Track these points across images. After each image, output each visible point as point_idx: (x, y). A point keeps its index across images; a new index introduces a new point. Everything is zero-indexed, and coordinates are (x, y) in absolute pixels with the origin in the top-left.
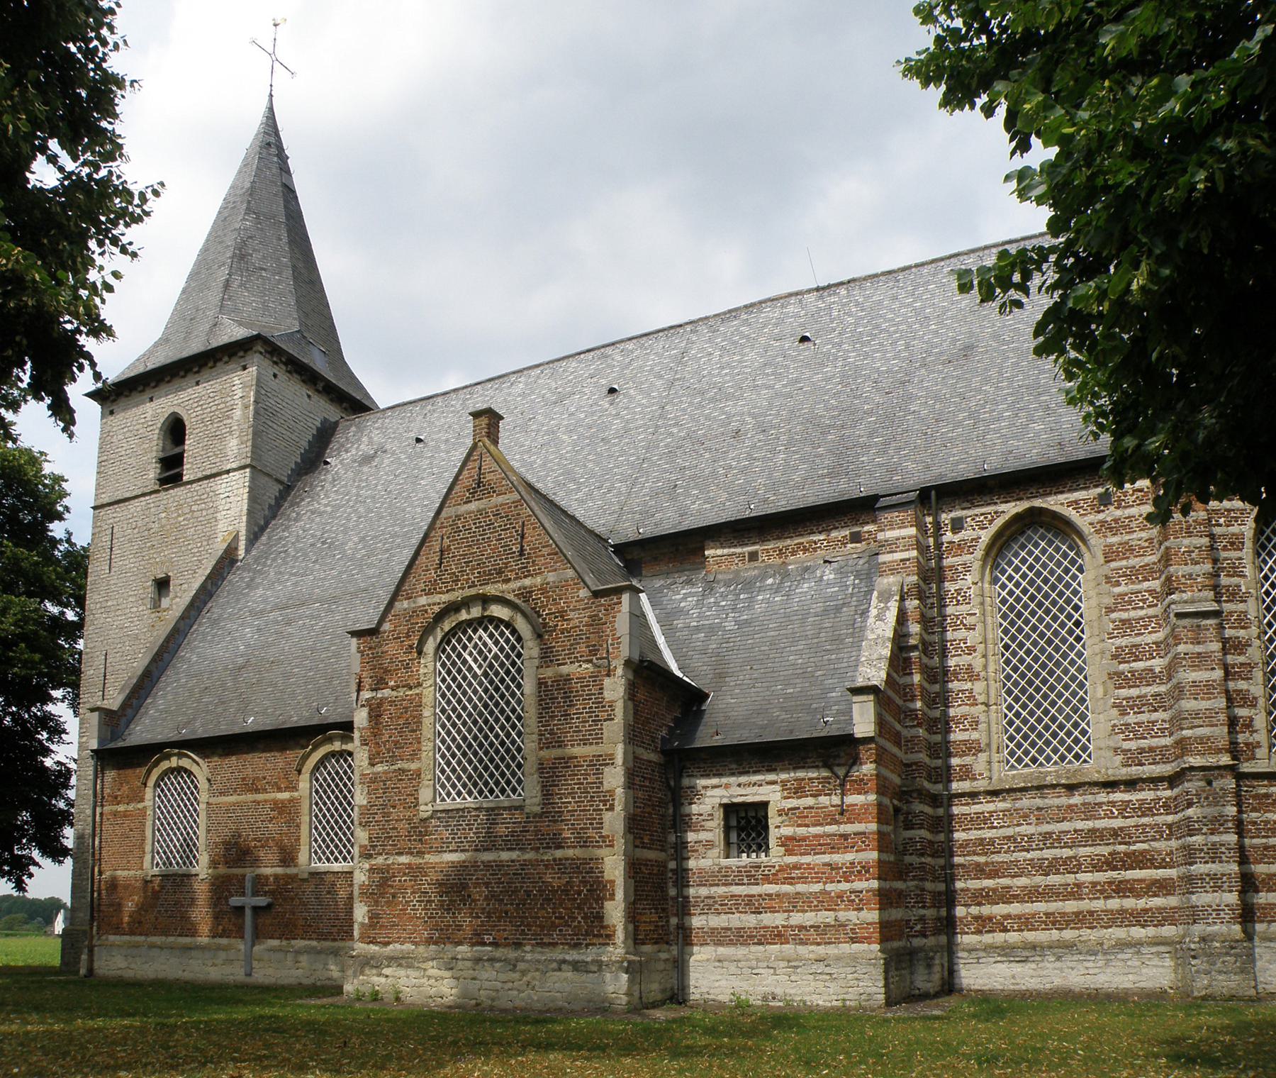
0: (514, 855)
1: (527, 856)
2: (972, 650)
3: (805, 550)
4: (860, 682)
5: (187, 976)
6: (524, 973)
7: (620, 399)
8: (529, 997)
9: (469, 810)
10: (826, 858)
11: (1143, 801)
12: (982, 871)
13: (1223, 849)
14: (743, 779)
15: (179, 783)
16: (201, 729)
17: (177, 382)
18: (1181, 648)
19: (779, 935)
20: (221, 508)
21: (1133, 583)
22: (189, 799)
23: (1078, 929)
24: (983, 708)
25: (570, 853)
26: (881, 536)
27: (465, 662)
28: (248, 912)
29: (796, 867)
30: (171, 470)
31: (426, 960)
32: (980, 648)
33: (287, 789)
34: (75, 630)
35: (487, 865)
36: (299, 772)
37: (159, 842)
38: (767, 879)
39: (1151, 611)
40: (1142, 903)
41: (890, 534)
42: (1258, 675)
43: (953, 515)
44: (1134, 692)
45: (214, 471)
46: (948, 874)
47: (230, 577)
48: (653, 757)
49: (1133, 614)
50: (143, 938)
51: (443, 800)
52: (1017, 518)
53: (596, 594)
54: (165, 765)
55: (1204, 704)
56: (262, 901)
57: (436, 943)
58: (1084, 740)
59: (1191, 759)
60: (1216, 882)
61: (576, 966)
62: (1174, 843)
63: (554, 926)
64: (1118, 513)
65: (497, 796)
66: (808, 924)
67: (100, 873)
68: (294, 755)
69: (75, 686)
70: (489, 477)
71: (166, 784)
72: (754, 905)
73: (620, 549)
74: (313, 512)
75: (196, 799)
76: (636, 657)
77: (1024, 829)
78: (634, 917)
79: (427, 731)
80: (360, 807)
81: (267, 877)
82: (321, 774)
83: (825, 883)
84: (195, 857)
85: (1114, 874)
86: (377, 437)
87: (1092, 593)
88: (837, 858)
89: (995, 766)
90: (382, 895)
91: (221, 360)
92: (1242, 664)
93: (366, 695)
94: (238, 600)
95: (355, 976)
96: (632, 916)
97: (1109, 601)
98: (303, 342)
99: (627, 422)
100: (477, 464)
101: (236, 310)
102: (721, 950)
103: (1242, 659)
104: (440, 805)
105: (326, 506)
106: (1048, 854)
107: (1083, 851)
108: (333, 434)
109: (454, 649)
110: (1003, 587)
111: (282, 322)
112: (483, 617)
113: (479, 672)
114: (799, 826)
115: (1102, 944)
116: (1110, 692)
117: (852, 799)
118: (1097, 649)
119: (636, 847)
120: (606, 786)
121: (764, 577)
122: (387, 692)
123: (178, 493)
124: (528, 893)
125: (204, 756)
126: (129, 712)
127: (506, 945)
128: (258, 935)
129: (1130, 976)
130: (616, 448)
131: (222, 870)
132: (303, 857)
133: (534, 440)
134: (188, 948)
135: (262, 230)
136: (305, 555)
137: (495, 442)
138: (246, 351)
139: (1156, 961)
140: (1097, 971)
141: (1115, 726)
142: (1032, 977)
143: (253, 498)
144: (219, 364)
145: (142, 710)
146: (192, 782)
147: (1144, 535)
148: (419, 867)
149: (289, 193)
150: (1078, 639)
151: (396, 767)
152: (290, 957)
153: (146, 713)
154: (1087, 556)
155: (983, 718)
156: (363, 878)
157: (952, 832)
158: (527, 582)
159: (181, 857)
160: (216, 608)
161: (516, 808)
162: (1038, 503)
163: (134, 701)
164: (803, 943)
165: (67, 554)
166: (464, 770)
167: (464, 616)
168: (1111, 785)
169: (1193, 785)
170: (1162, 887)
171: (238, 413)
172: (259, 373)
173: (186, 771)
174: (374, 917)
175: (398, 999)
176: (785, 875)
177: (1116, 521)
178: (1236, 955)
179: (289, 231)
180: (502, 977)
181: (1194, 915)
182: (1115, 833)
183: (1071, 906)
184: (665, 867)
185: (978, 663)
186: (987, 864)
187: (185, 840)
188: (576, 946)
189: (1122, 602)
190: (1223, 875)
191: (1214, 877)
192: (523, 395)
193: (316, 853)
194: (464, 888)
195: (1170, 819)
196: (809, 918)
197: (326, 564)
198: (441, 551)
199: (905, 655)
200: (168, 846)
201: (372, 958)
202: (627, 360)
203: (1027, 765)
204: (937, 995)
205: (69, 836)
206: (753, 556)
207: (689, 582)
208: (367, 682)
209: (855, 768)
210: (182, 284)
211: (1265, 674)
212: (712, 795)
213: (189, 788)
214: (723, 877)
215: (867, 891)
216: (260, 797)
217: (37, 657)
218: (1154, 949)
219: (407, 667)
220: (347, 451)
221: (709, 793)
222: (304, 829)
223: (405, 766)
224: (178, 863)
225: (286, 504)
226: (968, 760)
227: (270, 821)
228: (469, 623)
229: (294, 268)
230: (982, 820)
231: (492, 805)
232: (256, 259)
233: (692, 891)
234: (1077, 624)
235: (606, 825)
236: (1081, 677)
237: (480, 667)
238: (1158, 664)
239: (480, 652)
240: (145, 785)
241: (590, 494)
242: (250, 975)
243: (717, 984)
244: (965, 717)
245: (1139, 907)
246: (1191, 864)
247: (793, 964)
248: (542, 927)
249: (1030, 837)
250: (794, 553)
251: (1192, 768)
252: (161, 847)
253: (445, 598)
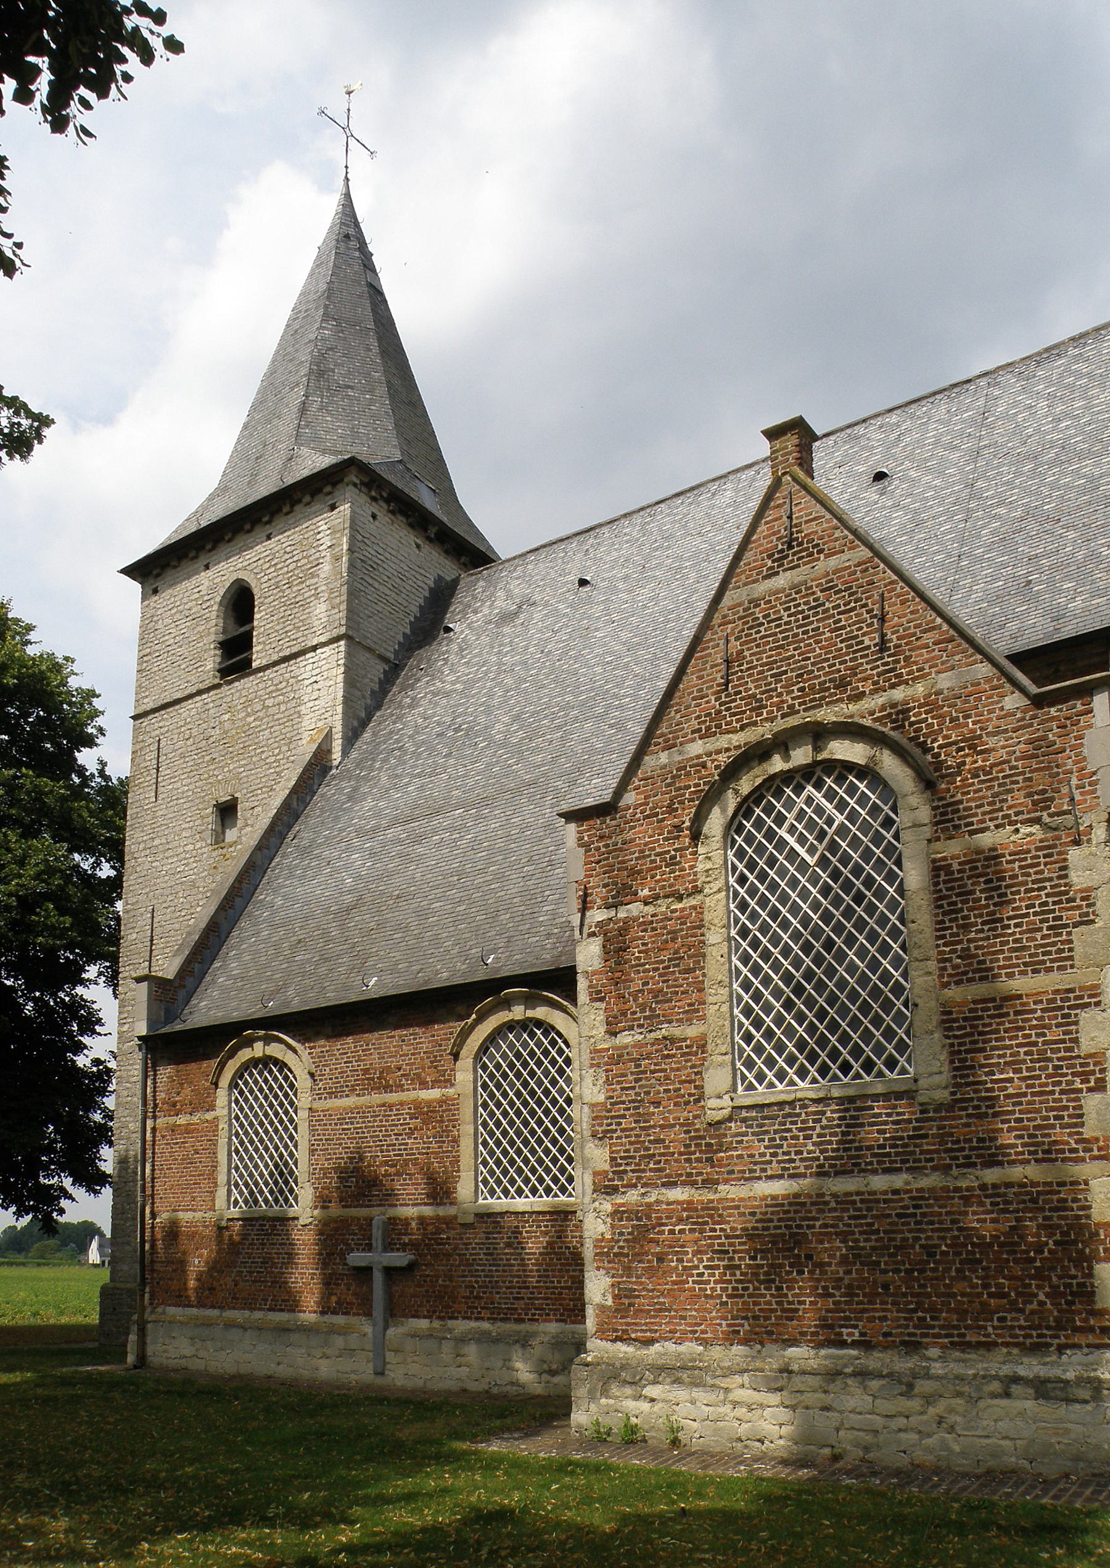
0: (899, 1181)
1: (924, 1182)
5: (283, 1371)
6: (929, 1400)
8: (944, 1445)
9: (803, 1103)
15: (266, 1081)
16: (296, 1001)
17: (240, 540)
22: (281, 1105)
25: (1017, 1173)
27: (781, 844)
28: (378, 1277)
30: (235, 656)
31: (730, 1372)
33: (436, 1084)
34: (115, 885)
35: (844, 1201)
36: (456, 1056)
37: (237, 1168)
45: (295, 650)
50: (215, 1312)
51: (750, 1087)
54: (245, 1055)
56: (399, 1259)
57: (745, 1342)
61: (1042, 1389)
63: (986, 1312)
65: (771, 1085)
67: (154, 1216)
68: (446, 1031)
69: (114, 959)
71: (246, 1083)
74: (435, 694)
75: (292, 1104)
81: (406, 1222)
82: (492, 1058)
84: (291, 1191)
86: (518, 589)
90: (639, 1256)
91: (299, 501)
93: (597, 915)
94: (337, 819)
95: (592, 1397)
98: (408, 476)
99: (916, 512)
100: (783, 512)
101: (316, 438)
104: (744, 1098)
105: (453, 683)
109: (759, 824)
111: (380, 448)
112: (815, 763)
113: (811, 861)
123: (247, 684)
125: (304, 1039)
126: (190, 981)
127: (885, 1348)
128: (395, 1311)
131: (335, 1210)
132: (464, 1189)
134: (283, 1330)
135: (345, 339)
136: (431, 749)
137: (810, 473)
138: (334, 485)
144: (297, 508)
145: (208, 978)
146: (286, 1078)
148: (708, 1207)
151: (658, 1035)
152: (447, 1347)
153: (214, 982)
156: (602, 1228)
158: (898, 694)
159: (271, 1192)
160: (304, 831)
161: (899, 1096)
165: (101, 790)
166: (790, 1032)
167: (777, 764)
171: (326, 568)
172: (353, 512)
173: (276, 1061)
174: (624, 1298)
175: (675, 1442)
179: (380, 340)
180: (886, 1406)
187: (276, 1166)
188: (1037, 1349)
193: (485, 1182)
194: (798, 1243)
197: (464, 757)
198: (728, 662)
200: (251, 1175)
201: (623, 1367)
202: (893, 437)
205: (108, 1159)
208: (598, 894)
213: (281, 1087)
216: (393, 1097)
217: (68, 921)
219: (672, 862)
220: (475, 612)
222: (466, 1146)
223: (676, 1031)
224: (266, 1201)
225: (395, 689)
227: (410, 1135)
228: (787, 777)
231: (851, 1092)
232: (338, 375)
237: (812, 850)
239: (811, 825)
240: (216, 1085)
242: (382, 1374)
248: (962, 1314)
252: (241, 1176)
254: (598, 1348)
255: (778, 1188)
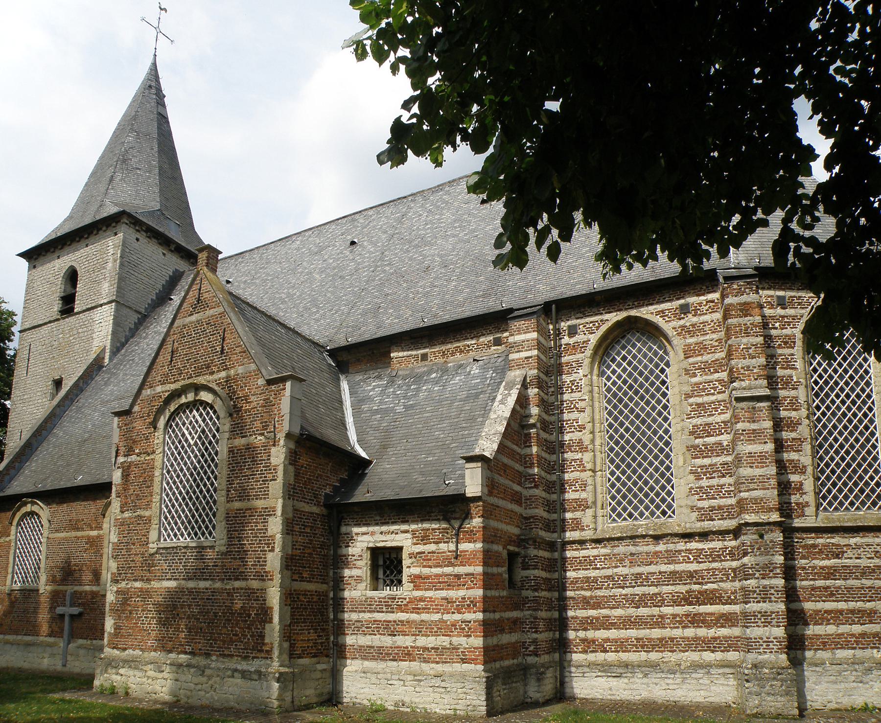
0: (207, 584)
2: (582, 428)
3: (461, 352)
4: (477, 451)
5: (26, 665)
6: (210, 677)
7: (357, 249)
8: (212, 697)
10: (443, 593)
11: (713, 550)
12: (588, 602)
13: (772, 591)
14: (384, 528)
17: (74, 245)
18: (740, 426)
19: (409, 654)
20: (96, 330)
21: (706, 374)
23: (662, 652)
24: (590, 473)
26: (511, 339)
28: (67, 619)
29: (422, 599)
32: (589, 426)
35: (191, 591)
38: (400, 609)
39: (720, 397)
40: (711, 633)
41: (518, 338)
42: (807, 448)
43: (569, 323)
44: (707, 461)
45: (93, 305)
46: (562, 604)
47: (98, 378)
48: (315, 509)
49: (706, 399)
51: (165, 540)
52: (618, 324)
53: (270, 382)
55: (758, 472)
56: (75, 610)
58: (669, 499)
59: (747, 517)
60: (767, 619)
61: (245, 675)
62: (737, 584)
63: (232, 641)
64: (695, 319)
65: (199, 538)
66: (430, 646)
70: (205, 295)
72: (391, 629)
73: (333, 353)
74: (155, 333)
76: (297, 431)
77: (621, 570)
78: (289, 637)
79: (156, 488)
80: (113, 543)
83: (443, 614)
85: (687, 608)
87: (675, 383)
88: (452, 594)
89: (600, 519)
91: (101, 229)
92: (793, 439)
93: (121, 459)
95: (102, 674)
96: (288, 634)
97: (687, 389)
99: (359, 264)
102: (367, 664)
103: (793, 435)
106: (639, 590)
107: (665, 589)
108: (179, 280)
110: (609, 378)
113: (192, 442)
114: (424, 567)
115: (680, 665)
116: (688, 461)
117: (464, 546)
118: (679, 427)
119: (294, 580)
120: (270, 533)
121: (430, 372)
122: (133, 458)
123: (71, 320)
124: (215, 614)
125: (48, 504)
126: (12, 472)
127: (200, 655)
128: (73, 636)
129: (702, 692)
130: (348, 282)
133: (298, 279)
134: (28, 645)
138: (117, 222)
139: (722, 681)
140: (676, 687)
141: (691, 488)
142: (625, 690)
143: (117, 323)
147: (715, 336)
149: (163, 120)
150: (666, 419)
151: (136, 514)
154: (671, 353)
155: (590, 481)
157: (565, 571)
162: (633, 313)
163: (17, 464)
164: (426, 661)
167: (183, 400)
168: (688, 536)
169: (748, 538)
170: (727, 620)
171: (110, 265)
173: (37, 514)
174: (117, 628)
175: (127, 693)
176: (413, 606)
177: (693, 325)
178: (782, 680)
179: (159, 144)
180: (196, 680)
181: (748, 645)
182: (691, 575)
183: (656, 633)
184: (327, 596)
185: (586, 438)
186: (591, 597)
188: (246, 658)
189: (698, 389)
190: (772, 613)
191: (764, 614)
192: (298, 249)
195: (735, 564)
196: (430, 641)
198: (172, 352)
199: (526, 432)
201: (113, 660)
203: (625, 519)
204: (547, 703)
206: (424, 357)
207: (379, 377)
208: (122, 450)
209: (467, 521)
210: (86, 180)
211: (813, 447)
212: (364, 539)
214: (367, 606)
215: (475, 622)
216: (79, 534)
218: (721, 671)
221: (360, 539)
226: (578, 514)
229: (161, 169)
230: (589, 563)
233: (346, 616)
234: (665, 407)
235: (268, 563)
236: (667, 450)
237: (193, 438)
238: (725, 439)
240: (11, 523)
241: (324, 315)
243: (362, 691)
244: (576, 480)
245: (710, 636)
246: (746, 603)
247: (418, 677)
248: (224, 642)
249: (625, 577)
250: (453, 354)
251: (747, 524)
253: (173, 387)
254: (108, 651)
255: (172, 584)
